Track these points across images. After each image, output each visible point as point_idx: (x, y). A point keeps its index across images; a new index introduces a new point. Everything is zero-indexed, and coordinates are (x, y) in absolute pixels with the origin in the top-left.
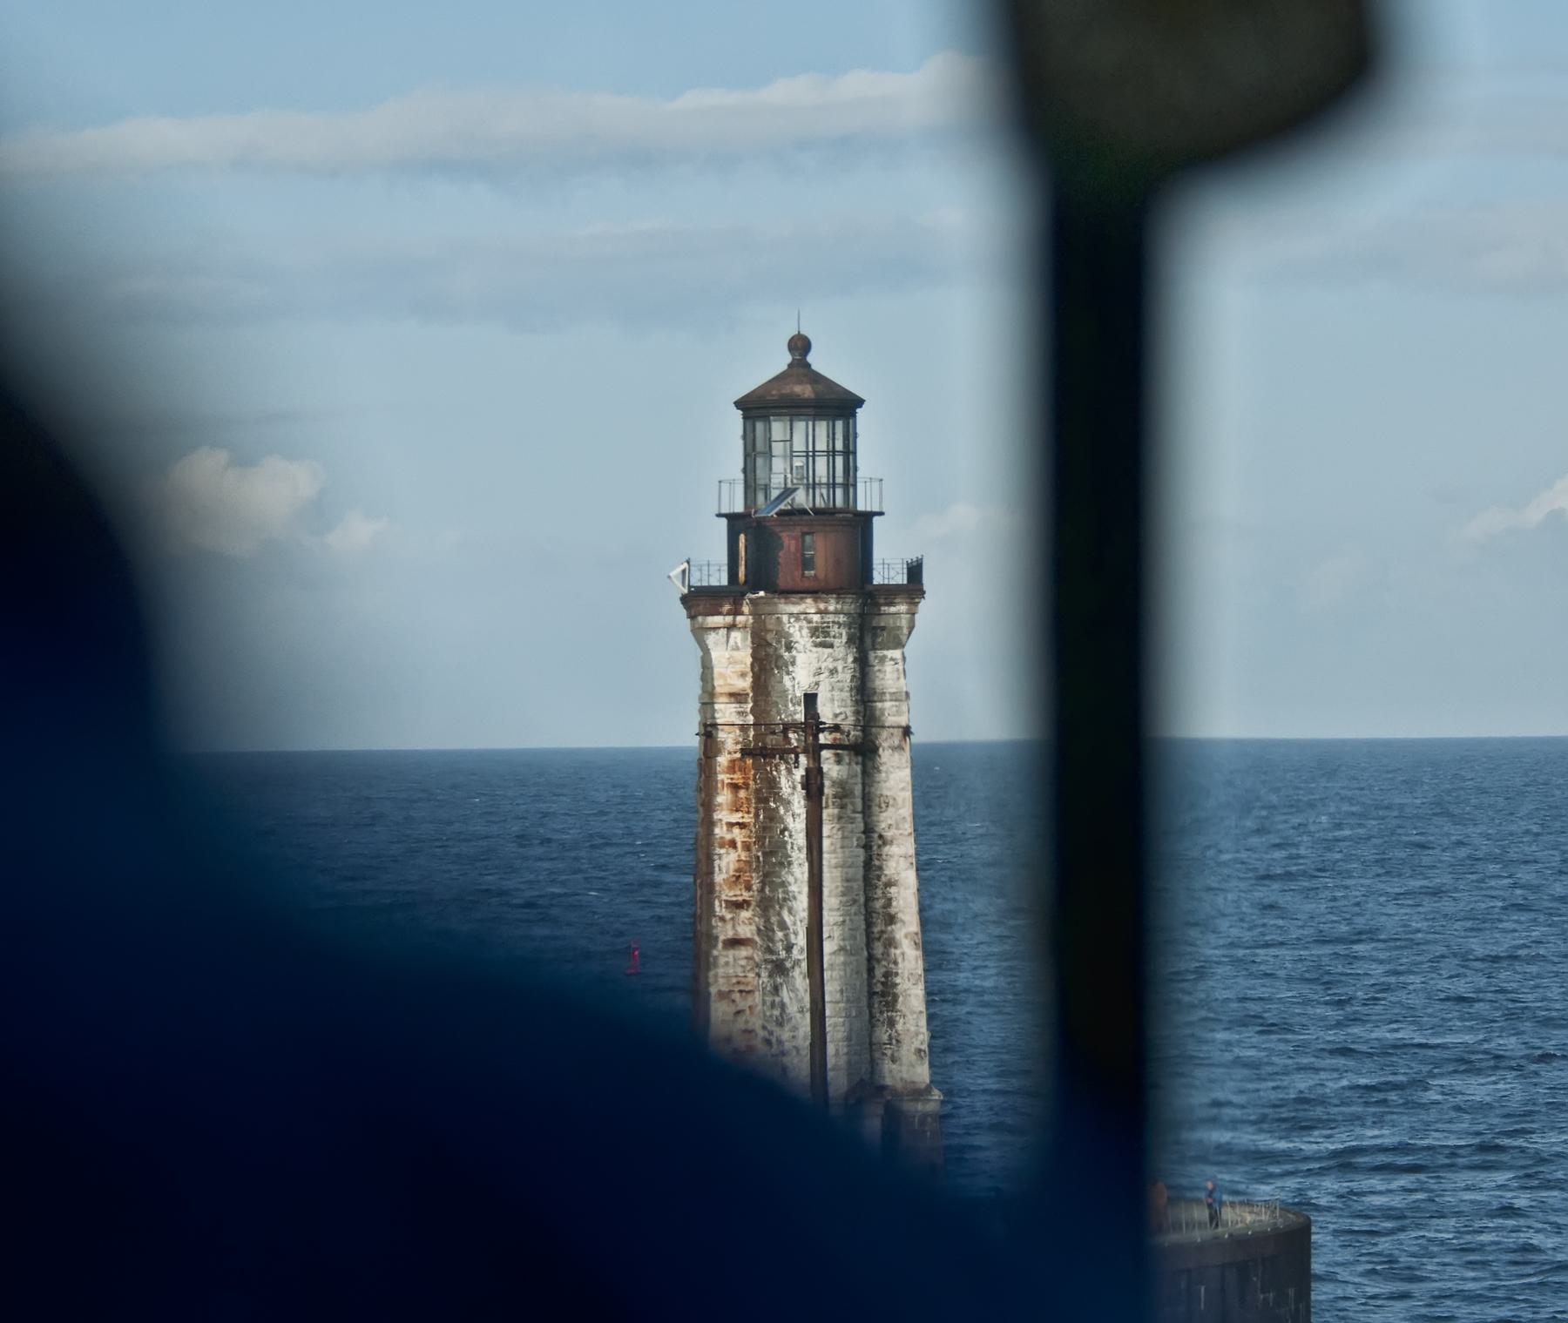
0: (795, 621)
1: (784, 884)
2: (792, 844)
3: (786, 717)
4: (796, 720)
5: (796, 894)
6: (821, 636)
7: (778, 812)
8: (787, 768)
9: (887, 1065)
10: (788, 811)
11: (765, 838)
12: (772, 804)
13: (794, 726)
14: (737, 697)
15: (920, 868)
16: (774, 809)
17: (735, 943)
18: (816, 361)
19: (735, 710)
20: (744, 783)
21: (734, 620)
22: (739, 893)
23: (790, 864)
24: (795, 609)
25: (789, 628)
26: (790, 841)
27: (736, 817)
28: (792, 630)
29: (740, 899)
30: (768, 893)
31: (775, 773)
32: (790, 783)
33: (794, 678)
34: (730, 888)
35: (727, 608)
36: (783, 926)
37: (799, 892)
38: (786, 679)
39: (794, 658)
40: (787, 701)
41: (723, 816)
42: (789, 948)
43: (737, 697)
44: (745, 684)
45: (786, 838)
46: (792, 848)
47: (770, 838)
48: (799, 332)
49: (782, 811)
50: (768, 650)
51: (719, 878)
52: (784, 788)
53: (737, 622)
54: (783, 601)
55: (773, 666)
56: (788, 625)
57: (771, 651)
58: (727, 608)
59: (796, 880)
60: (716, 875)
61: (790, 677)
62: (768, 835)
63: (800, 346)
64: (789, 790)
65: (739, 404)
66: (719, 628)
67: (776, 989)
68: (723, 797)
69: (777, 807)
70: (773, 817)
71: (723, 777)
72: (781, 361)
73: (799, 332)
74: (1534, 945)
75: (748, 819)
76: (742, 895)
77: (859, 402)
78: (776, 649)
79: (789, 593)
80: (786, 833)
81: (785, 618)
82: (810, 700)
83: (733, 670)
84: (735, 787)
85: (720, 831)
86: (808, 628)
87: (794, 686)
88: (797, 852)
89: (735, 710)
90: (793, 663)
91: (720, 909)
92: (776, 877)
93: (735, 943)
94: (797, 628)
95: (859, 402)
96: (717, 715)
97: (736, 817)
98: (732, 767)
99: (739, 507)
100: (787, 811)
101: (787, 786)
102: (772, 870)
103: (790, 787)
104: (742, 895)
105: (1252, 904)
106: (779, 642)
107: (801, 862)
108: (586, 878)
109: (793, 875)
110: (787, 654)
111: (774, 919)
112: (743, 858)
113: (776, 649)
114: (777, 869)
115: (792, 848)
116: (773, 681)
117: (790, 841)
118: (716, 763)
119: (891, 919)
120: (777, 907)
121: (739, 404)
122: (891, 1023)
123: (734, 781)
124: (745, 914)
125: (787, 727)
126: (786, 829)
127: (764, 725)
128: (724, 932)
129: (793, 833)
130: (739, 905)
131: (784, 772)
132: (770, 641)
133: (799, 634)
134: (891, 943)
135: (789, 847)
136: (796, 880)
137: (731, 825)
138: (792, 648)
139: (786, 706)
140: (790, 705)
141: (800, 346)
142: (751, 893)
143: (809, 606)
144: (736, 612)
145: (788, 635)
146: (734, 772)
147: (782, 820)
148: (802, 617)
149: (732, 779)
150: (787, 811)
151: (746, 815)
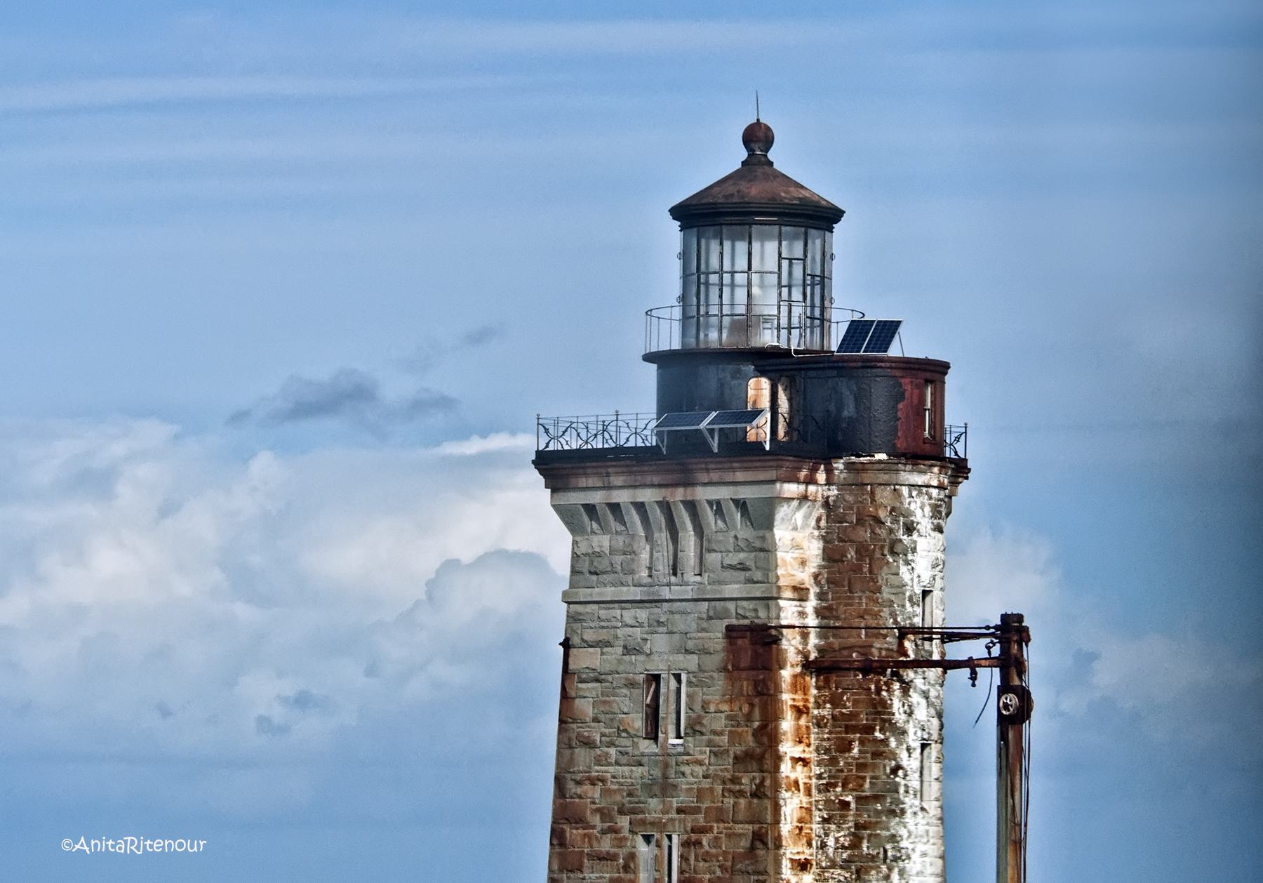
0: (918, 495)
1: (893, 838)
2: (906, 786)
3: (904, 620)
4: (914, 624)
5: (910, 852)
7: (888, 745)
8: (901, 687)
10: (902, 745)
11: (864, 778)
12: (877, 734)
16: (882, 740)
19: (796, 609)
20: (804, 706)
21: (806, 490)
22: (800, 850)
23: (903, 812)
24: (919, 479)
25: (909, 504)
26: (903, 782)
28: (913, 507)
29: (802, 857)
30: (865, 849)
31: (884, 693)
32: (906, 707)
33: (913, 568)
34: (795, 843)
35: (803, 474)
37: (913, 850)
38: (904, 569)
39: (915, 542)
40: (905, 599)
41: (789, 749)
43: (800, 593)
45: (897, 779)
46: (907, 792)
47: (872, 778)
48: (758, 120)
49: (893, 743)
50: (878, 531)
52: (897, 714)
53: (809, 493)
54: (909, 467)
55: (886, 552)
56: (908, 500)
57: (882, 533)
58: (803, 474)
59: (910, 834)
60: (781, 825)
61: (910, 567)
62: (868, 775)
64: (904, 717)
66: (793, 499)
69: (887, 739)
72: (734, 157)
73: (758, 120)
75: (811, 754)
76: (803, 853)
78: (891, 531)
80: (900, 773)
81: (905, 490)
83: (794, 555)
84: (799, 711)
86: (930, 505)
87: (912, 579)
88: (912, 796)
89: (796, 609)
90: (914, 550)
91: (786, 866)
92: (882, 829)
94: (919, 504)
96: (782, 615)
100: (900, 743)
101: (901, 710)
102: (873, 820)
103: (905, 712)
104: (803, 853)
106: (895, 521)
107: (915, 809)
109: (905, 827)
110: (905, 537)
112: (805, 805)
113: (891, 531)
114: (884, 818)
115: (907, 792)
116: (883, 575)
117: (903, 782)
118: (781, 678)
120: (884, 868)
123: (795, 703)
126: (899, 767)
127: (866, 628)
129: (909, 773)
131: (897, 693)
132: (883, 520)
135: (902, 790)
136: (910, 834)
137: (796, 760)
138: (915, 529)
139: (903, 606)
140: (908, 604)
142: (811, 850)
145: (908, 514)
146: (796, 692)
147: (894, 756)
148: (924, 490)
149: (794, 700)
150: (900, 743)
151: (807, 749)
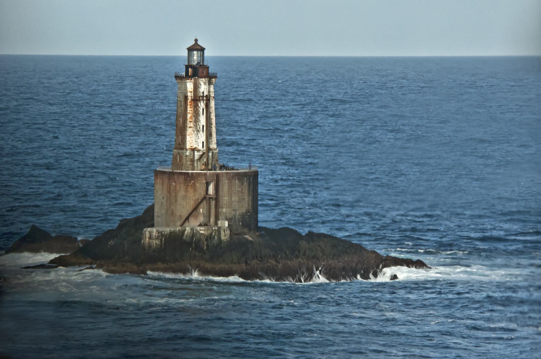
6: (205, 83)
9: (211, 145)
13: (201, 96)
14: (191, 92)
15: (216, 117)
17: (190, 127)
18: (199, 43)
27: (191, 109)
36: (199, 125)
42: (200, 128)
43: (191, 92)
44: (192, 90)
51: (188, 118)
63: (196, 40)
65: (187, 49)
67: (198, 134)
68: (189, 106)
70: (197, 109)
71: (189, 103)
72: (194, 42)
74: (364, 351)
77: (205, 49)
79: (201, 77)
82: (203, 92)
85: (188, 111)
91: (188, 122)
93: (190, 127)
95: (205, 49)
97: (191, 109)
98: (190, 102)
99: (187, 64)
105: (312, 81)
108: (366, 83)
111: (197, 124)
119: (212, 124)
121: (187, 49)
122: (211, 139)
124: (192, 123)
125: (200, 97)
128: (189, 126)
130: (191, 122)
133: (202, 83)
134: (211, 127)
141: (196, 40)
143: (204, 79)
144: (191, 80)
